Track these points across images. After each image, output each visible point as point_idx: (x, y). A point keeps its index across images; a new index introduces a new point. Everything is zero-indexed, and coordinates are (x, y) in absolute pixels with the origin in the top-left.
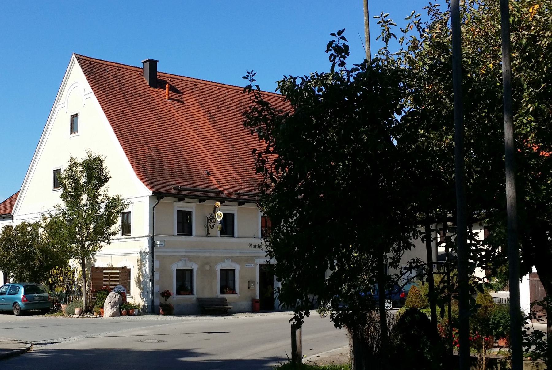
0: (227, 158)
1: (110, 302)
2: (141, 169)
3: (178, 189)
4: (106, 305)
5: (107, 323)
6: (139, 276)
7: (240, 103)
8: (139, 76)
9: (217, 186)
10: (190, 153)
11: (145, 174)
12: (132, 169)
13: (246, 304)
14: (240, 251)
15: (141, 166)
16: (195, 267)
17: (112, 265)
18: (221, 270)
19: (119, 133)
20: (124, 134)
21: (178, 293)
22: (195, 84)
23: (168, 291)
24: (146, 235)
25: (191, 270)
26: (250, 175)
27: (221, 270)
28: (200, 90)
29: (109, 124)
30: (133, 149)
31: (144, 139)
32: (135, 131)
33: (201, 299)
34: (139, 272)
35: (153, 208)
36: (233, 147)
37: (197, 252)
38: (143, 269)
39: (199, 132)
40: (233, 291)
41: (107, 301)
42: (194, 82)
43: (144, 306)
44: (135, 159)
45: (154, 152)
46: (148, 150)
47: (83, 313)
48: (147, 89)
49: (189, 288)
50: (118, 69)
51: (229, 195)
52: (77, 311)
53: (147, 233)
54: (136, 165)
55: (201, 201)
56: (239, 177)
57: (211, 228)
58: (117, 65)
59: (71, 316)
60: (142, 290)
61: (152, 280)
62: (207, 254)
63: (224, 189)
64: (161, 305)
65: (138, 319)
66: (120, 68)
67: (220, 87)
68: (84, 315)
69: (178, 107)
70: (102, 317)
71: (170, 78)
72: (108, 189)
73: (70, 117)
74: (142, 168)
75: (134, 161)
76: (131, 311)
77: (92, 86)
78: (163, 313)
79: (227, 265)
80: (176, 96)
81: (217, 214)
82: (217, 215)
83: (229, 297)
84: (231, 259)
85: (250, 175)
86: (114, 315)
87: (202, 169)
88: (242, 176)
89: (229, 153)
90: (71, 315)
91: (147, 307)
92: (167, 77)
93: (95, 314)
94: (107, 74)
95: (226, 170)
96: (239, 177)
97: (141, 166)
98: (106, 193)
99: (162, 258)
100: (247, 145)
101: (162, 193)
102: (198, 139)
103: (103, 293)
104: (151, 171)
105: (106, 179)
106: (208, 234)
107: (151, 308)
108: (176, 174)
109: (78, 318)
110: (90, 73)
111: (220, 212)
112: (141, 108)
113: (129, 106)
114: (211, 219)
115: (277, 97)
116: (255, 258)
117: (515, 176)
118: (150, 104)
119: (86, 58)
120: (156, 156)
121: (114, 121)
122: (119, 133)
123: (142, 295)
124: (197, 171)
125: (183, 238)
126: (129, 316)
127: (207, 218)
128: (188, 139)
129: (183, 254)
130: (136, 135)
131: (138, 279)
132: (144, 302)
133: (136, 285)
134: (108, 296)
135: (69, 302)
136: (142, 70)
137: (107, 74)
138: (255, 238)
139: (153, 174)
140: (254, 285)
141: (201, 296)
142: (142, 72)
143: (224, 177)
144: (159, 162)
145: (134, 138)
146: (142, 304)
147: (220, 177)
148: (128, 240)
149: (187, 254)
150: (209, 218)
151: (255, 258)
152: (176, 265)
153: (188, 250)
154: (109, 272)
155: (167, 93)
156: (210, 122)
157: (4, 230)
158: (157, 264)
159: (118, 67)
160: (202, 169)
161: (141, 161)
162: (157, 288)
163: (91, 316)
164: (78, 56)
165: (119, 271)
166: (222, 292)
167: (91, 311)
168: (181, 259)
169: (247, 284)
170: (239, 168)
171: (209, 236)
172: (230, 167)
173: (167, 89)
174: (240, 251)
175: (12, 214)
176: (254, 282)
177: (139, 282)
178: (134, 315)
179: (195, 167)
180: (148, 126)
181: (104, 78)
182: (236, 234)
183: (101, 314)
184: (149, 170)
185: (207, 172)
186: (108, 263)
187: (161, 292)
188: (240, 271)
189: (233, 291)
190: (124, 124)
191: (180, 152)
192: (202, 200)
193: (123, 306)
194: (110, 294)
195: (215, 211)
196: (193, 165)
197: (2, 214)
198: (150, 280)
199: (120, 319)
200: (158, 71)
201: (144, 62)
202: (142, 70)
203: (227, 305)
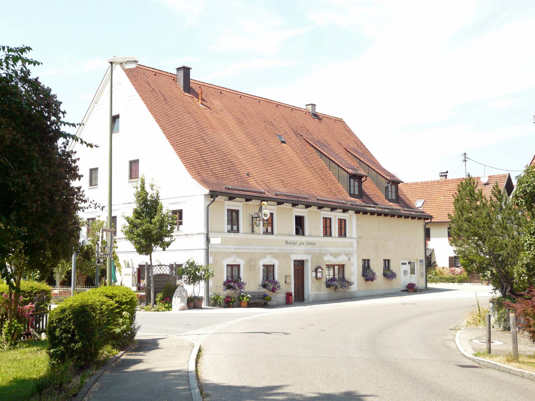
16: (241, 262)
22: (221, 91)
39: (180, 146)
42: (220, 90)
55: (247, 200)
57: (257, 226)
79: (268, 261)
99: (216, 253)
106: (253, 231)
129: (233, 251)
136: (175, 76)
142: (175, 78)
149: (236, 251)
176: (290, 276)
185: (247, 173)
188: (278, 266)
200: (191, 78)
201: (178, 69)
202: (175, 76)
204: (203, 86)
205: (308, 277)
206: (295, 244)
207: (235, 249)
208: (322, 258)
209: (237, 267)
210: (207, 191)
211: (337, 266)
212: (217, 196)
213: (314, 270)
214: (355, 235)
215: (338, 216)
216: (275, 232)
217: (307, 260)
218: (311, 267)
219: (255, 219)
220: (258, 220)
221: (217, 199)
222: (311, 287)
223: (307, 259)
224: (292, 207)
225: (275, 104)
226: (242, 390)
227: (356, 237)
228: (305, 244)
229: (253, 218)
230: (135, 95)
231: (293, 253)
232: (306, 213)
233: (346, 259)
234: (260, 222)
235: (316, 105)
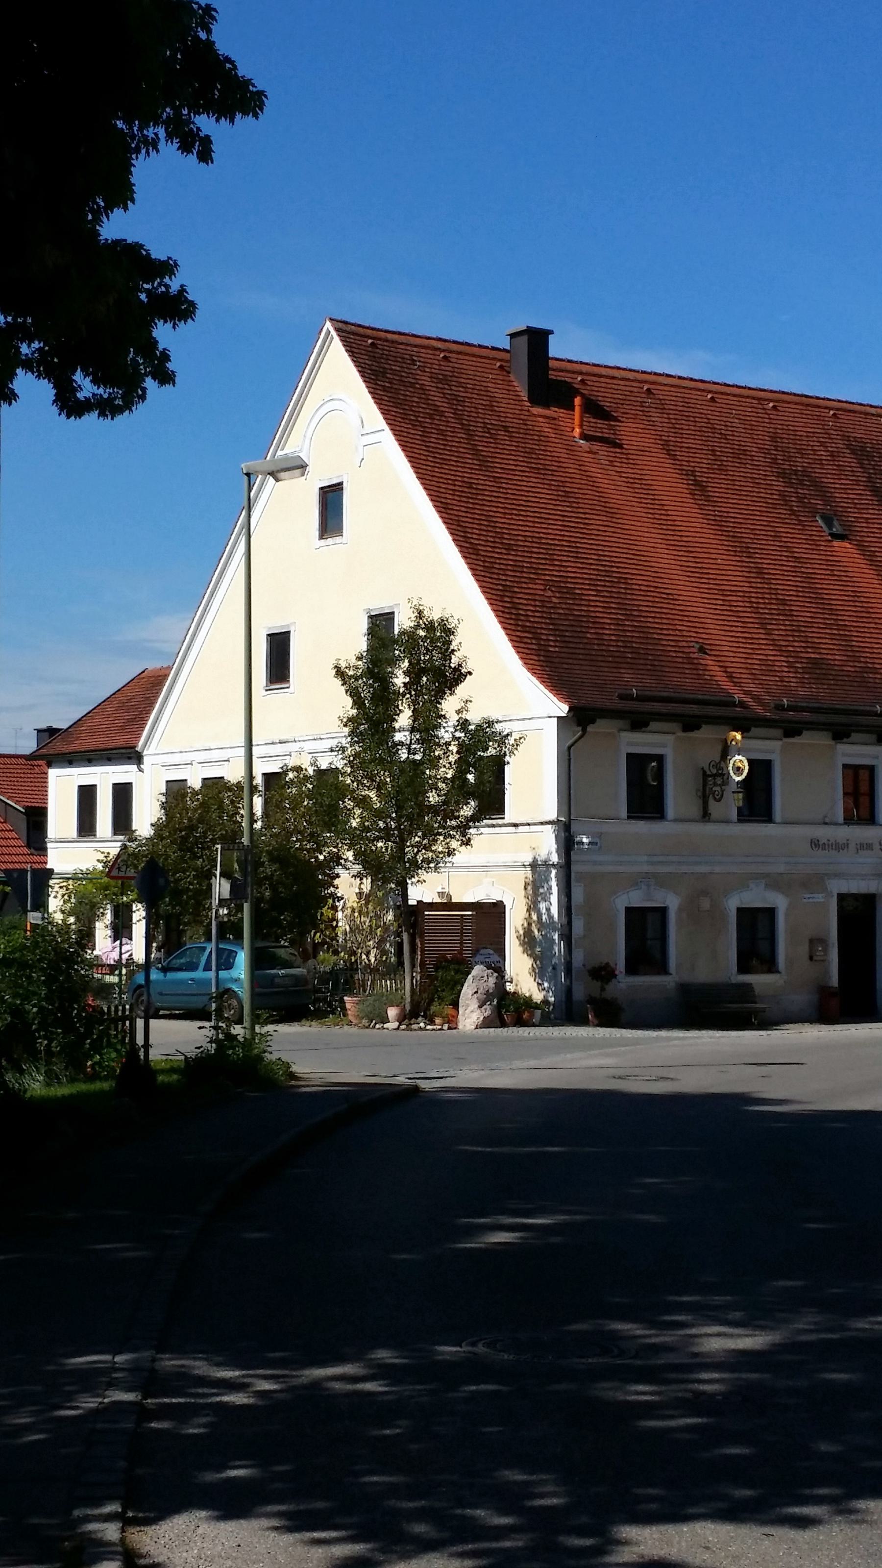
0: (747, 605)
1: (476, 992)
2: (532, 644)
3: (629, 697)
4: (467, 999)
5: (468, 1041)
6: (530, 924)
7: (774, 439)
8: (499, 372)
9: (727, 685)
10: (649, 594)
11: (542, 658)
12: (509, 645)
13: (801, 999)
15: (530, 636)
16: (672, 902)
17: (449, 896)
18: (739, 910)
19: (468, 545)
20: (480, 548)
21: (632, 968)
23: (607, 964)
25: (662, 912)
26: (810, 650)
27: (739, 910)
28: (662, 407)
29: (440, 521)
30: (506, 588)
31: (531, 557)
32: (506, 536)
34: (530, 915)
35: (569, 748)
36: (760, 572)
38: (543, 906)
40: (770, 966)
41: (467, 990)
42: (646, 382)
44: (513, 617)
45: (558, 595)
46: (544, 590)
47: (408, 1017)
48: (524, 412)
50: (445, 358)
51: (759, 710)
52: (392, 1012)
53: (553, 815)
54: (518, 634)
56: (783, 659)
57: (715, 799)
58: (439, 345)
59: (377, 1026)
60: (538, 962)
61: (567, 937)
63: (746, 693)
64: (591, 1000)
65: (550, 1034)
66: (451, 352)
67: (716, 393)
68: (411, 1024)
69: (609, 461)
70: (455, 1028)
71: (581, 373)
72: (469, 705)
73: (317, 491)
74: (534, 641)
75: (512, 622)
76: (526, 1016)
77: (385, 413)
80: (600, 427)
81: (732, 762)
82: (731, 765)
83: (759, 980)
84: (764, 881)
85: (810, 650)
86: (486, 1023)
87: (685, 639)
88: (789, 654)
89: (752, 590)
90: (376, 1024)
92: (574, 372)
93: (438, 1021)
94: (419, 372)
95: (745, 638)
96: (783, 659)
97: (530, 636)
98: (464, 715)
100: (797, 564)
101: (594, 710)
102: (666, 551)
103: (454, 969)
104: (557, 649)
105: (458, 676)
107: (564, 1007)
108: (618, 654)
109: (399, 1032)
110: (374, 372)
111: (740, 757)
112: (513, 467)
113: (484, 464)
114: (714, 776)
115: (873, 415)
116: (826, 878)
117: (718, 1395)
118: (534, 456)
119: (361, 330)
120: (564, 606)
121: (452, 512)
122: (468, 545)
123: (540, 973)
124: (673, 643)
125: (641, 827)
126: (521, 1026)
127: (704, 772)
128: (642, 553)
129: (646, 868)
130: (509, 547)
131: (528, 932)
132: (544, 993)
133: (520, 949)
134: (470, 976)
135: (365, 991)
136: (507, 356)
137: (419, 372)
138: (826, 824)
139: (563, 655)
140: (826, 951)
142: (507, 361)
143: (743, 660)
144: (573, 623)
145: (505, 557)
146: (538, 997)
147: (733, 660)
148: (497, 830)
151: (826, 878)
152: (625, 897)
153: (655, 859)
154: (462, 915)
155: (577, 421)
156: (695, 499)
157: (164, 800)
158: (578, 894)
159: (444, 351)
160: (685, 639)
161: (530, 621)
162: (578, 957)
163: (429, 1027)
164: (340, 325)
165: (470, 913)
166: (743, 968)
167: (425, 1013)
168: (636, 881)
169: (804, 949)
170: (781, 633)
171: (709, 821)
172: (755, 631)
173: (577, 409)
175: (138, 749)
177: (528, 941)
178: (534, 1025)
179: (665, 632)
180: (537, 520)
181: (412, 385)
182: (778, 814)
183: (452, 1022)
184: (551, 646)
185: (697, 646)
186: (440, 890)
188: (787, 915)
189: (770, 966)
190: (476, 516)
191: (623, 591)
192: (690, 724)
193: (508, 1002)
194: (474, 973)
195: (726, 752)
196: (662, 629)
197: (103, 746)
198: (561, 937)
199: (505, 1034)
200: (550, 355)
201: (513, 336)
202: (507, 356)
203: (755, 1003)
204: (594, 375)
210: (563, 709)
212: (593, 722)
220: (719, 782)
221: (590, 729)
224: (833, 743)
225: (830, 409)
226: (34, 754)
229: (705, 775)
230: (383, 430)
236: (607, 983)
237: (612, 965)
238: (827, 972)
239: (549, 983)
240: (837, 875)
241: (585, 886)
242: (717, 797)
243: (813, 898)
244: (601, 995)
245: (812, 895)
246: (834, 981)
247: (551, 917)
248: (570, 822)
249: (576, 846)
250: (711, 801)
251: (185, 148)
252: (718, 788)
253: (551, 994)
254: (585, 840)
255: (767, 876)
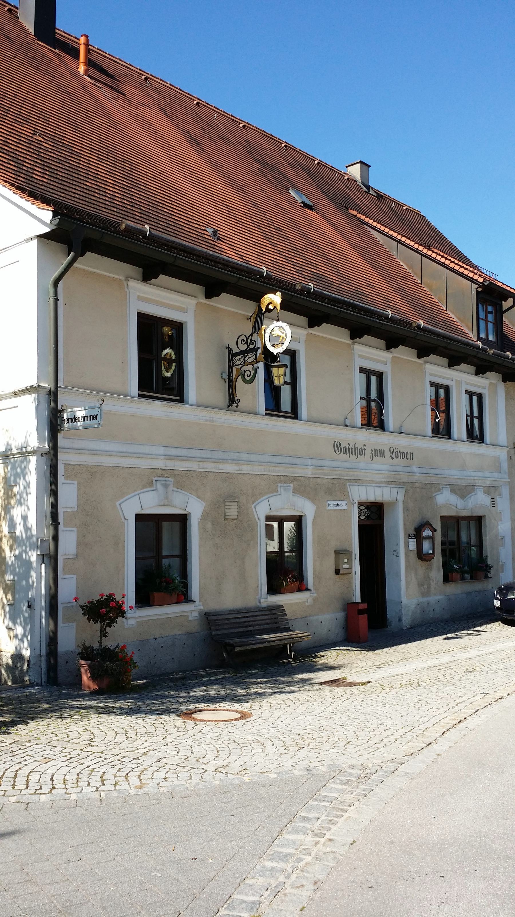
14: (315, 462)
24: (28, 385)
33: (216, 614)
36: (255, 205)
37: (203, 459)
38: (17, 513)
43: (17, 657)
49: (176, 576)
57: (245, 381)
60: (9, 596)
62: (230, 468)
78: (94, 686)
91: (29, 661)
107: (44, 665)
114: (243, 353)
129: (160, 464)
138: (346, 426)
140: (350, 560)
141: (213, 605)
149: (170, 465)
150: (235, 350)
153: (173, 452)
174: (315, 462)
176: (348, 553)
187: (83, 601)
198: (42, 556)
203: (288, 629)
205: (396, 552)
206: (360, 452)
207: (169, 457)
208: (431, 498)
209: (177, 525)
211: (292, 524)
213: (412, 531)
214: (503, 438)
215: (467, 383)
216: (304, 410)
217: (393, 504)
218: (405, 524)
219: (238, 360)
220: (250, 360)
222: (407, 582)
223: (393, 498)
227: (505, 444)
228: (387, 454)
229: (232, 355)
231: (357, 481)
232: (389, 364)
233: (486, 500)
234: (256, 365)
235: (370, 166)
236: (109, 625)
237: (118, 597)
238: (350, 584)
239: (24, 628)
240: (357, 481)
241: (79, 484)
242: (248, 379)
243: (337, 505)
244: (100, 642)
245: (336, 502)
246: (357, 598)
247: (27, 529)
248: (57, 391)
249: (66, 425)
250: (240, 384)
251: (31, 387)
252: (250, 367)
253: (26, 644)
254: (80, 413)
255: (293, 479)
